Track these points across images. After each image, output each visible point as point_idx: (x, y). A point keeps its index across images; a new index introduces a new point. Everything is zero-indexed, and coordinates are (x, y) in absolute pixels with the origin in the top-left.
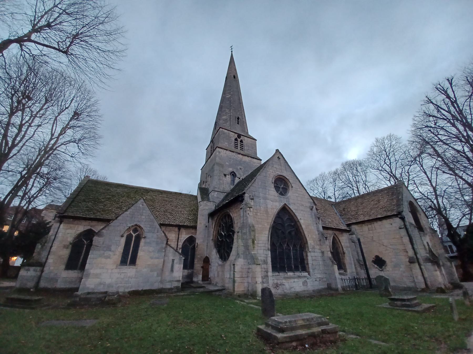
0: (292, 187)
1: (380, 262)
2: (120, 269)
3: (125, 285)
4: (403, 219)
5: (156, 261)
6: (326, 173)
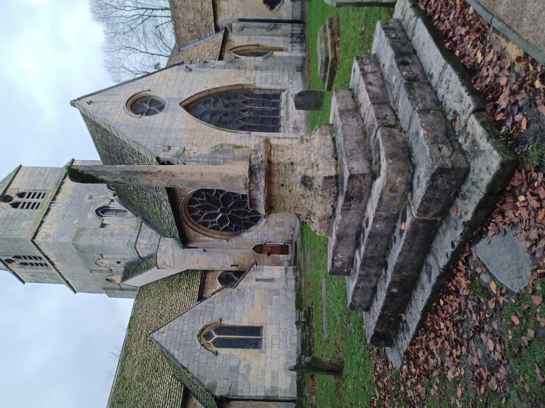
0: (150, 90)
2: (266, 347)
3: (288, 336)
6: (107, 58)
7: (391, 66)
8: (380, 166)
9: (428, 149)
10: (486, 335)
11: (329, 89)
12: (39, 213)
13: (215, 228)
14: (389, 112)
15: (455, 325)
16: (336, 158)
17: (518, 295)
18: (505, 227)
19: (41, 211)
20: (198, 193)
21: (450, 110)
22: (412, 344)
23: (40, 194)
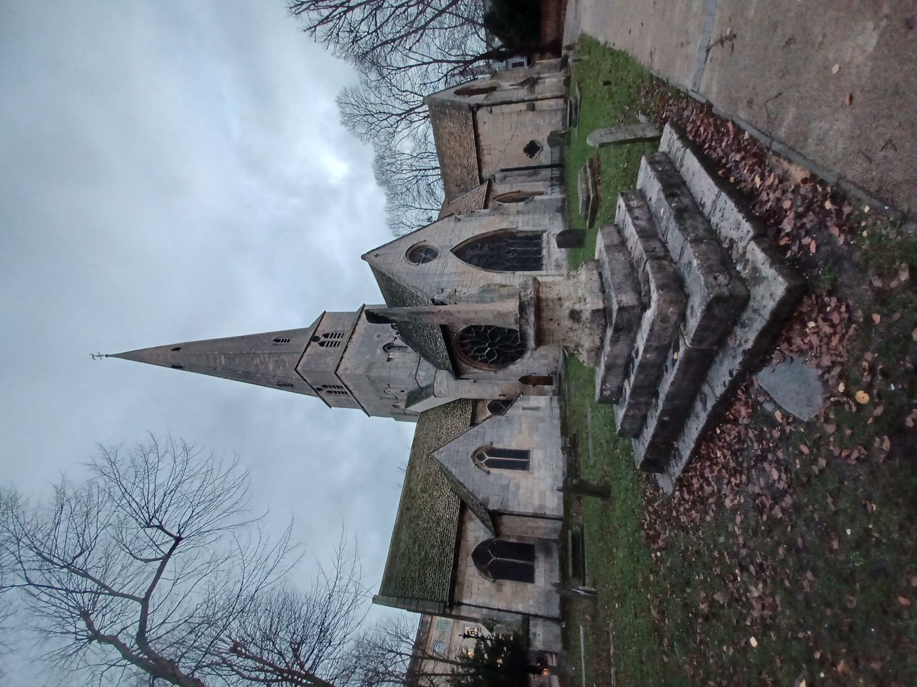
1: (532, 149)
4: (479, 106)
6: (389, 216)
7: (659, 199)
8: (650, 298)
9: (702, 278)
10: (770, 464)
11: (591, 226)
12: (340, 349)
13: (484, 361)
14: (657, 245)
15: (734, 453)
16: (604, 292)
17: (808, 423)
18: (791, 355)
19: (340, 349)
20: (468, 330)
21: (726, 238)
22: (685, 470)
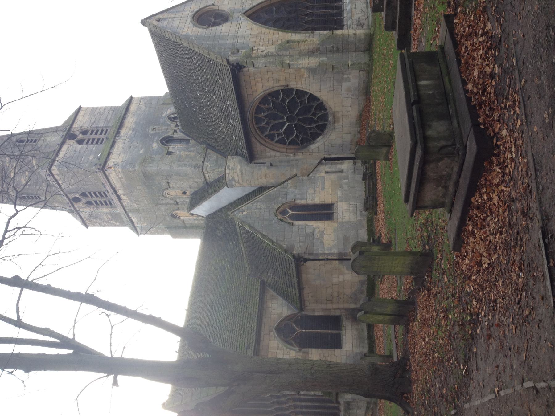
5: (328, 184)
23: (102, 131)
